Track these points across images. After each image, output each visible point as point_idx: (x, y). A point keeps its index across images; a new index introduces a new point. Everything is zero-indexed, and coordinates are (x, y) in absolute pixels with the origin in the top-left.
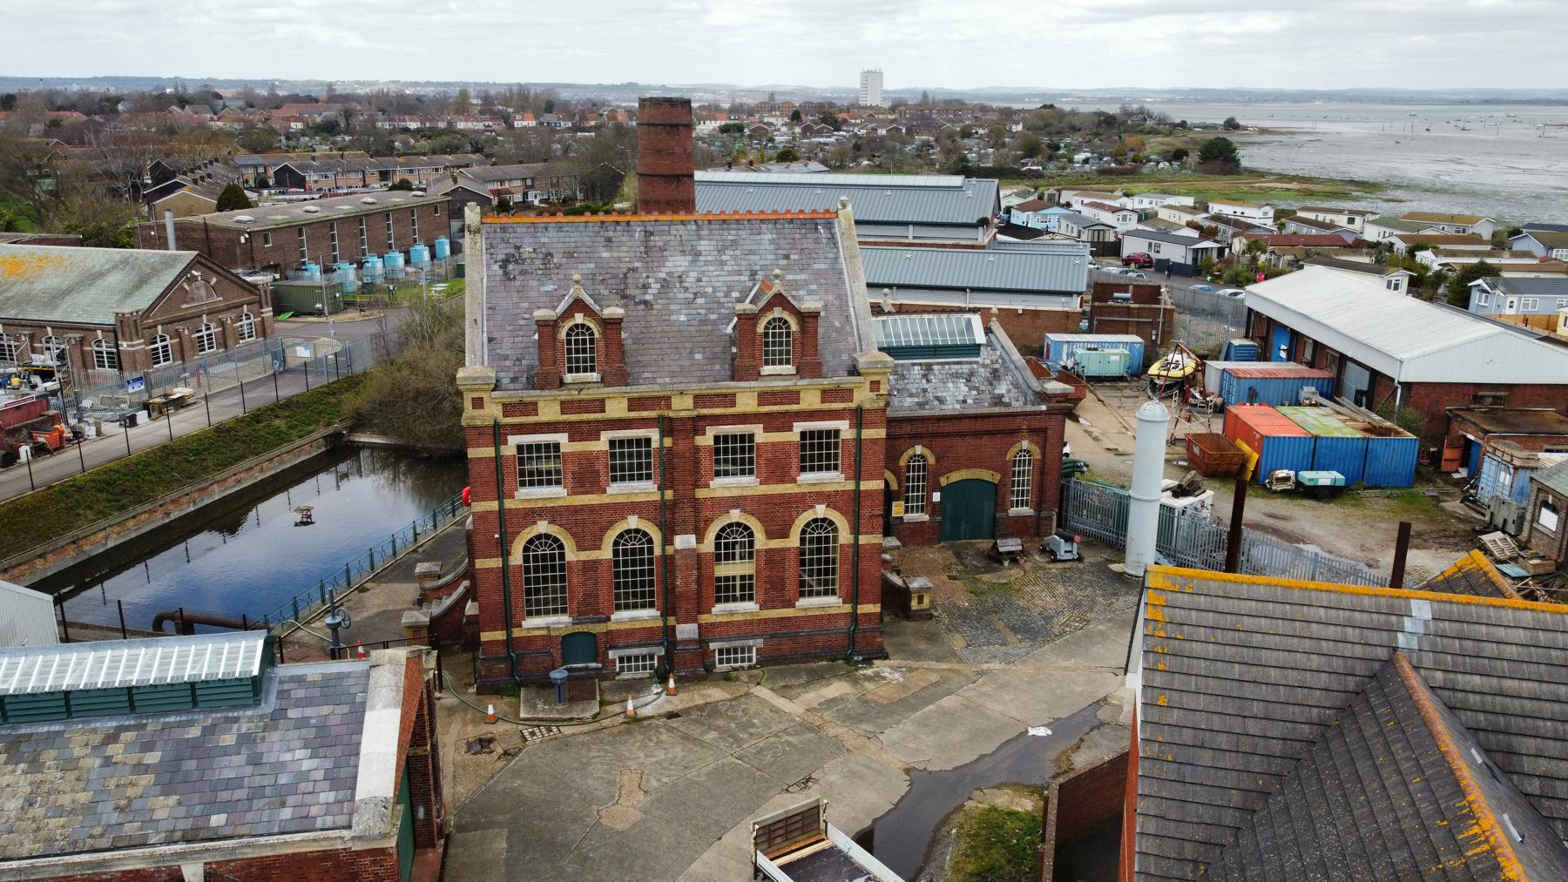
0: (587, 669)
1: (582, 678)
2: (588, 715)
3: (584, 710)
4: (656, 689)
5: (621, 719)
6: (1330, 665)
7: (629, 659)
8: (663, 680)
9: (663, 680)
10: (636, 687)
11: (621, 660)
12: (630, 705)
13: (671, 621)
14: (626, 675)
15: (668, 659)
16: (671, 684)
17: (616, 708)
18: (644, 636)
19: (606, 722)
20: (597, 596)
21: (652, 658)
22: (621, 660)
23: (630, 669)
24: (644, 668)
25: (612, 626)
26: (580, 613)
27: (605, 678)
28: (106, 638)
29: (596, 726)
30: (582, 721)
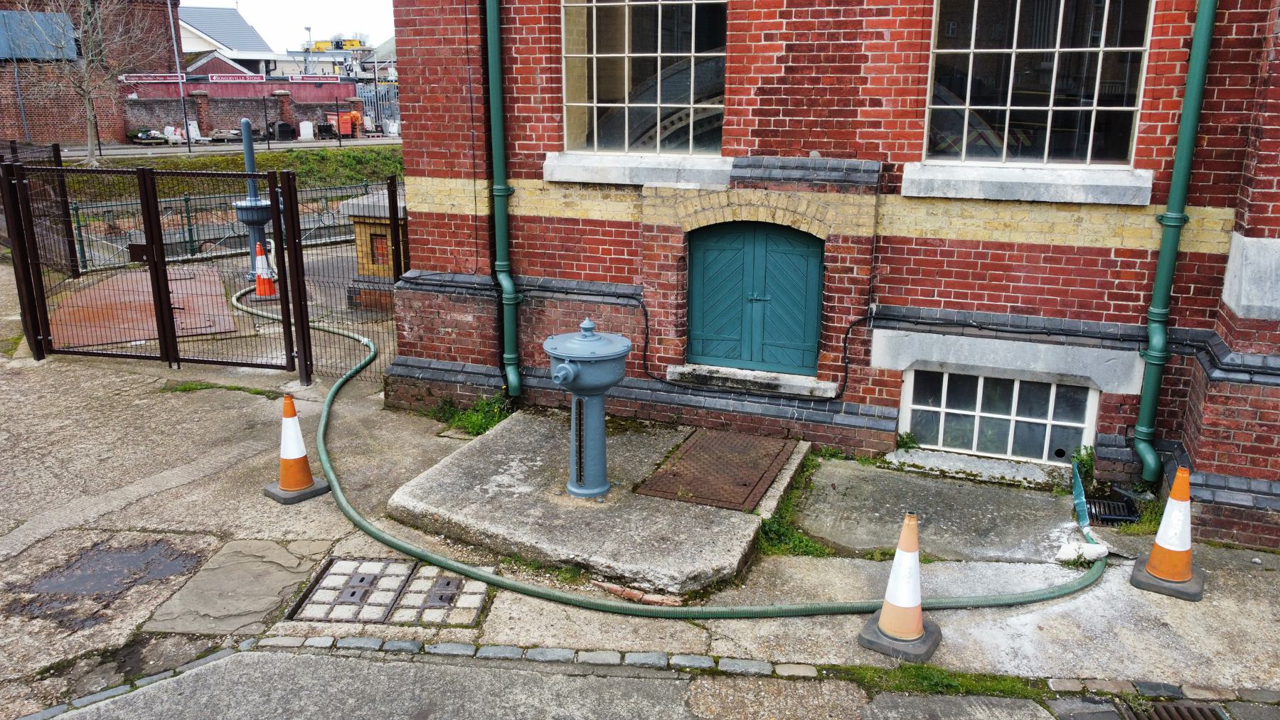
0: (770, 391)
1: (752, 426)
2: (668, 570)
3: (662, 544)
4: (1078, 540)
5: (835, 644)
6: (1213, 494)
7: (963, 386)
8: (1120, 500)
9: (1120, 500)
10: (966, 515)
11: (927, 383)
12: (904, 585)
13: (1209, 228)
14: (938, 457)
15: (1164, 417)
16: (1175, 526)
17: (835, 581)
18: (1068, 290)
19: (741, 641)
20: (849, 63)
21: (1072, 397)
22: (927, 383)
23: (959, 438)
24: (1028, 443)
25: (904, 220)
26: (769, 141)
27: (845, 448)
28: (205, 166)
29: (682, 642)
30: (627, 598)
